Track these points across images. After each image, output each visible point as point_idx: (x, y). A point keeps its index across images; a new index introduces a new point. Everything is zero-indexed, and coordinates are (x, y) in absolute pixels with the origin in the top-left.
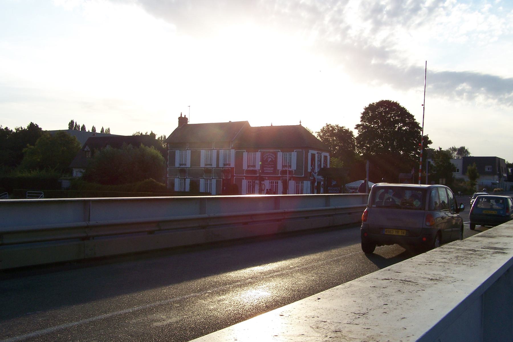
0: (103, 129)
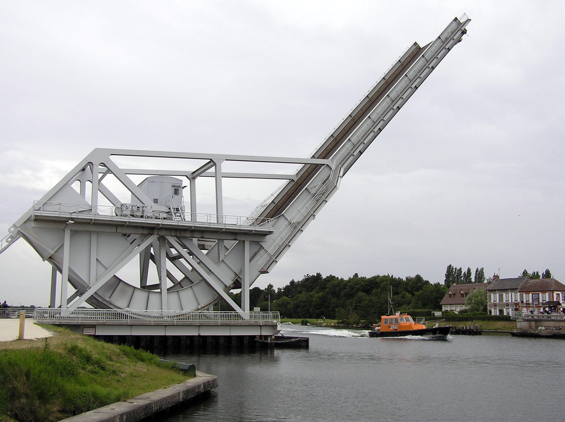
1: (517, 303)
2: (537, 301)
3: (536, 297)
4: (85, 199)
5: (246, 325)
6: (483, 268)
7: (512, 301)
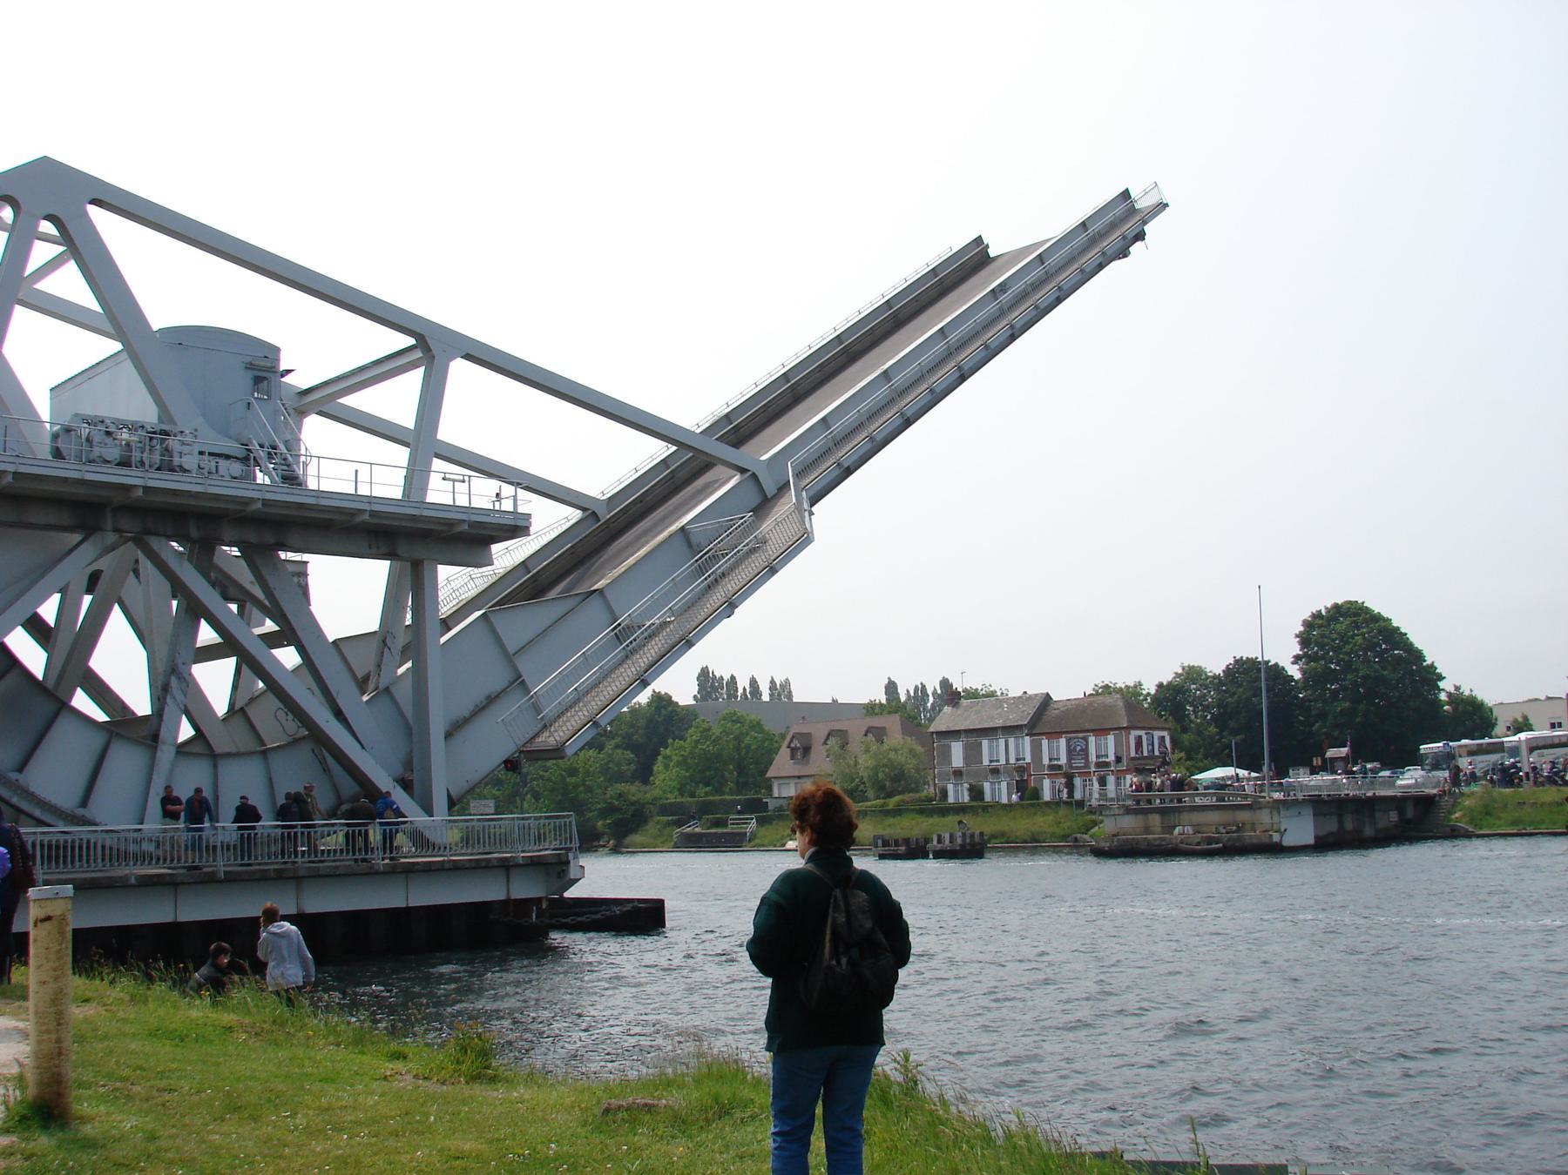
0: (773, 682)
1: (1024, 767)
2: (1082, 759)
3: (1079, 748)
4: (462, 357)
5: (341, 871)
6: (733, 678)
7: (1007, 760)
